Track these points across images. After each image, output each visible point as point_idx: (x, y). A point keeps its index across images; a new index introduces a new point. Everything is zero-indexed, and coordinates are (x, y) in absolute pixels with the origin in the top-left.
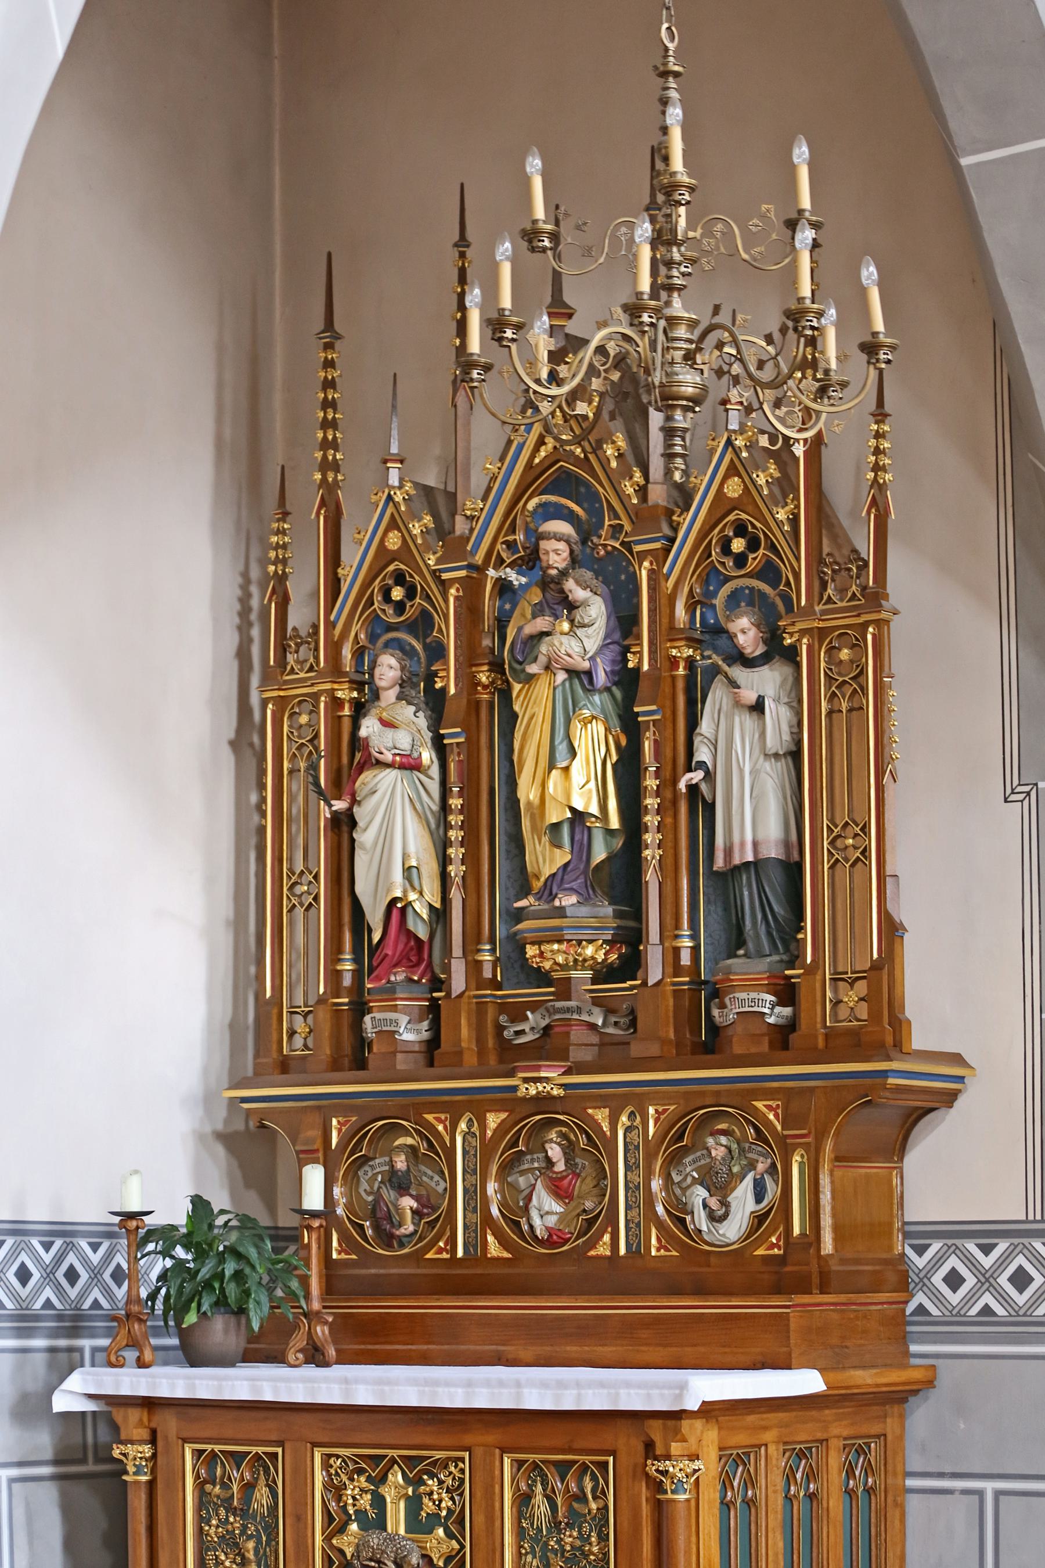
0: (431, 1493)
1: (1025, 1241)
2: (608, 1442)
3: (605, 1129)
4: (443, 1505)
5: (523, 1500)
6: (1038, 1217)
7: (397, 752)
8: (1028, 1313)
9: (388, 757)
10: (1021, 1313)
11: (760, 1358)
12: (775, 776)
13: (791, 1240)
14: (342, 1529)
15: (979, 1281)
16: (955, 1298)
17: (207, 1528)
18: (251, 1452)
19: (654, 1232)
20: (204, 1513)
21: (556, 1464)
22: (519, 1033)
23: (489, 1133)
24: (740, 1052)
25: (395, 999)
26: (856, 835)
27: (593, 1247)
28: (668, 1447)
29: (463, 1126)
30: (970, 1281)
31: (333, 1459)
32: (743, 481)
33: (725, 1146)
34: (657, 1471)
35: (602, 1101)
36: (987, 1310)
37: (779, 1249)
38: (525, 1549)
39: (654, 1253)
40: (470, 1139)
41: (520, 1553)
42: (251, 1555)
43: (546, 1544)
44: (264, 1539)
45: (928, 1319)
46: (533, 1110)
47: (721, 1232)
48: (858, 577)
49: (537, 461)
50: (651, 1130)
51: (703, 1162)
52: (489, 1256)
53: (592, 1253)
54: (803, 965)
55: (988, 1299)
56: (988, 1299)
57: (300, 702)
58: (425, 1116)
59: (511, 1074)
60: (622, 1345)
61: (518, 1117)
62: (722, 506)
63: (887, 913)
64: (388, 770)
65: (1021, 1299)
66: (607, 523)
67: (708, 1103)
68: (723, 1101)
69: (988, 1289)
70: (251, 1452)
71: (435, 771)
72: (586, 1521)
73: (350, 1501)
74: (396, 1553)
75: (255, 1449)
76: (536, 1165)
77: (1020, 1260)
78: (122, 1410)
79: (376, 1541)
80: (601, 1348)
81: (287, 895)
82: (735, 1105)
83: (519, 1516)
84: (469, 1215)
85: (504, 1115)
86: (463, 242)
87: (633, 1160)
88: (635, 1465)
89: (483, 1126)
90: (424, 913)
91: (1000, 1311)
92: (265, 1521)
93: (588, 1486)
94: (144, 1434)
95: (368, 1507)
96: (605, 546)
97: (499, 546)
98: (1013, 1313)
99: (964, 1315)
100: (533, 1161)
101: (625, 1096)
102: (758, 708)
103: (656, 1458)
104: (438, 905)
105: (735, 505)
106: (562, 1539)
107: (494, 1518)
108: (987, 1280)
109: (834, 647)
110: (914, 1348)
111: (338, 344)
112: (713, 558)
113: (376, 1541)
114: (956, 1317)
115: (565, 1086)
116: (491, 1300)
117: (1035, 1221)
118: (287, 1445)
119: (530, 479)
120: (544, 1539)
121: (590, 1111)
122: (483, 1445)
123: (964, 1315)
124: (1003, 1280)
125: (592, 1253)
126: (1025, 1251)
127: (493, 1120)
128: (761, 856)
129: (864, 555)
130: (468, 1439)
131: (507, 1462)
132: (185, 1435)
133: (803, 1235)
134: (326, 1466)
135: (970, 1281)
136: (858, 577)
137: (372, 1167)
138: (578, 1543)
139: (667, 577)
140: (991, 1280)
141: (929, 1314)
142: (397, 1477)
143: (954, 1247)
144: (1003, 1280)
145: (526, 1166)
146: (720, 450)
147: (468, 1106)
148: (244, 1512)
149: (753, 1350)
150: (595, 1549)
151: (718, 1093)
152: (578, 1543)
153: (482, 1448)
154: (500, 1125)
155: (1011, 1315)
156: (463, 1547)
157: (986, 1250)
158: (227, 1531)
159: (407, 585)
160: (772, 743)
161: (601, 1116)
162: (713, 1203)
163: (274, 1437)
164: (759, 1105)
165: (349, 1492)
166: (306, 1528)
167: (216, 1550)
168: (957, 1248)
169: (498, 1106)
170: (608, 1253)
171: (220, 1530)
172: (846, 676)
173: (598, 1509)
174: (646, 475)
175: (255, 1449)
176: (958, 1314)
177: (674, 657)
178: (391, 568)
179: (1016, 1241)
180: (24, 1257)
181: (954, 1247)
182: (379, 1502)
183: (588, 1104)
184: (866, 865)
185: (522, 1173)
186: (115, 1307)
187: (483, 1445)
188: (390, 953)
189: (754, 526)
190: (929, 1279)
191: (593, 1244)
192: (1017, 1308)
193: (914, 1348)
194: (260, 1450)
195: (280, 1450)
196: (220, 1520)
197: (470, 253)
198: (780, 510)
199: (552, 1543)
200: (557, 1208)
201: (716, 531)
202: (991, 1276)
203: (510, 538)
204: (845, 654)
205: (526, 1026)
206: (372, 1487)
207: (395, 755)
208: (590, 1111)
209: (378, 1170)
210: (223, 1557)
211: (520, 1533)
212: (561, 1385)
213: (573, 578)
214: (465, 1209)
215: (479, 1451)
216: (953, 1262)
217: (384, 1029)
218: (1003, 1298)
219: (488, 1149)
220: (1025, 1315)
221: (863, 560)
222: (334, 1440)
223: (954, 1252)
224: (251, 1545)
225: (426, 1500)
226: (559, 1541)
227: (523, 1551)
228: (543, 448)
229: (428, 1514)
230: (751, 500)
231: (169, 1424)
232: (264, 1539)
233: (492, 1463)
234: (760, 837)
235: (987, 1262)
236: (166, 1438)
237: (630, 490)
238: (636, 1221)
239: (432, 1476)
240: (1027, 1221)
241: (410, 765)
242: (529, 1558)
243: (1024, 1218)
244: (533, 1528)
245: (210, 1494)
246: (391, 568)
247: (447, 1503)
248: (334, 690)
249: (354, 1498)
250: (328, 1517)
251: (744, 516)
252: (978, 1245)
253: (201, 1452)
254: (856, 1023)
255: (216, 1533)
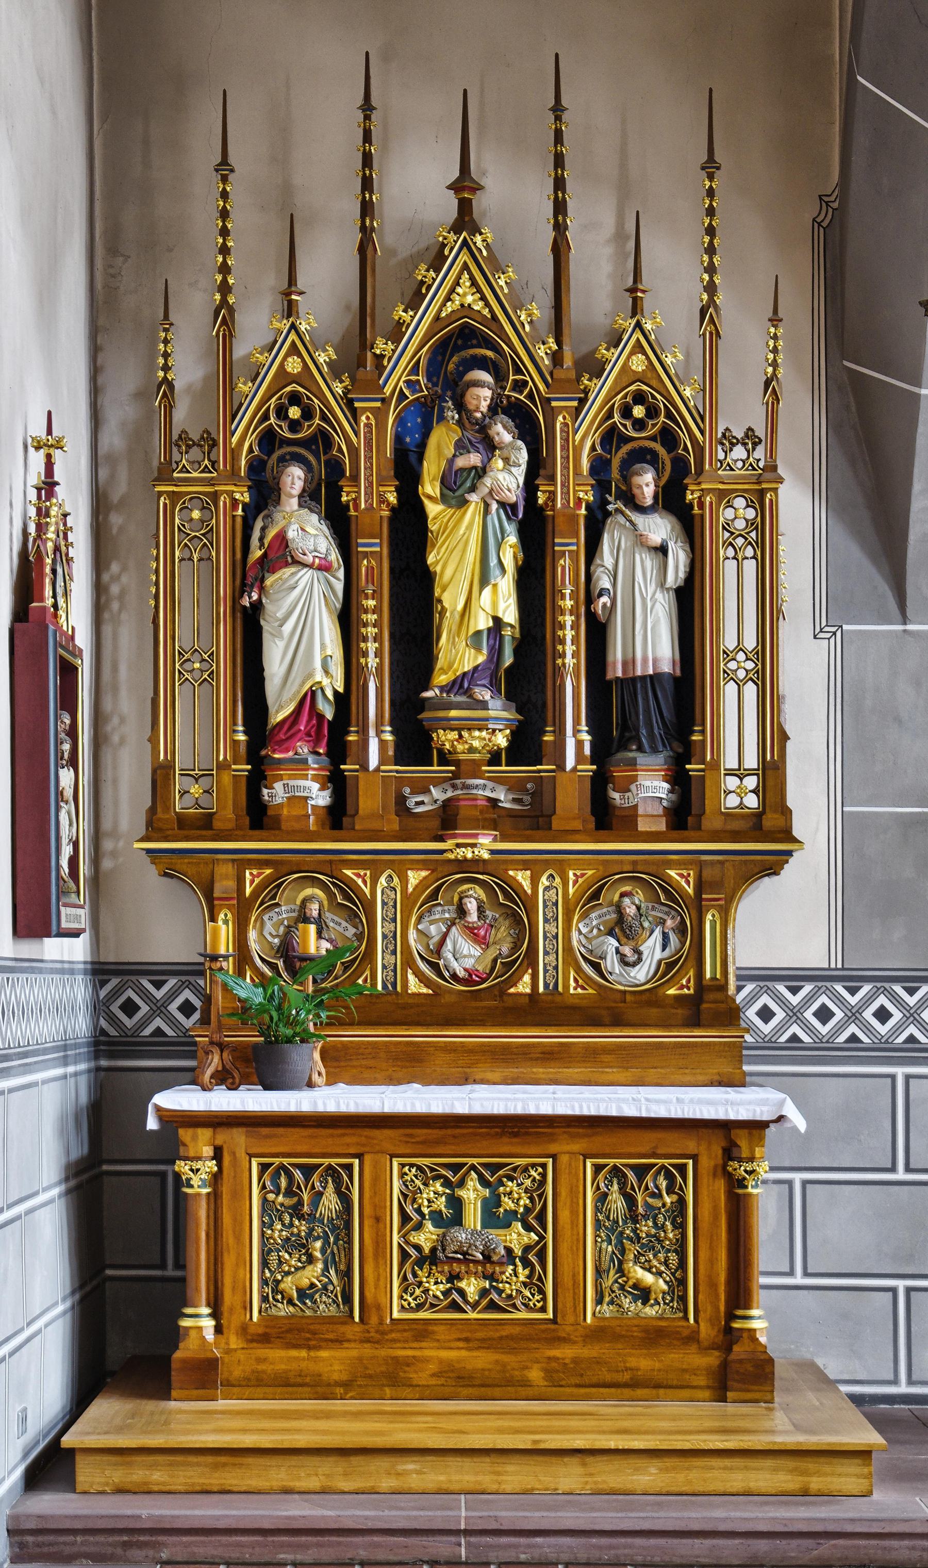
0: (511, 1193)
1: (828, 984)
2: (553, 1148)
3: (526, 888)
4: (522, 1203)
5: (602, 1198)
6: (839, 966)
7: (317, 554)
8: (890, 1041)
9: (309, 559)
10: (824, 1040)
11: (717, 1078)
12: (667, 606)
13: (704, 983)
14: (419, 1227)
15: (788, 1015)
16: (767, 1028)
17: (269, 1232)
18: (273, 1164)
19: (572, 973)
20: (266, 1219)
21: (632, 1167)
22: (418, 804)
23: (410, 889)
24: (643, 829)
25: (637, 771)
26: (203, 660)
27: (515, 985)
28: (752, 1151)
29: (383, 881)
30: (780, 1015)
31: (407, 1168)
32: (648, 358)
33: (636, 906)
34: (746, 1171)
35: (525, 866)
36: (853, 1038)
37: (689, 989)
38: (601, 1237)
39: (572, 991)
40: (389, 892)
41: (596, 1241)
42: (318, 1254)
43: (622, 1233)
44: (332, 1239)
45: (917, 1046)
46: (457, 870)
47: (632, 975)
48: (186, 453)
49: (443, 314)
50: (571, 891)
51: (608, 917)
52: (410, 992)
53: (512, 990)
54: (703, 761)
55: (795, 1029)
56: (795, 1029)
57: (191, 499)
58: (344, 871)
59: (441, 839)
60: (586, 1067)
61: (440, 875)
62: (283, 376)
63: (780, 724)
64: (306, 570)
65: (824, 1030)
66: (511, 378)
67: (625, 870)
68: (640, 868)
69: (795, 1022)
70: (273, 1164)
71: (341, 574)
72: (660, 1213)
73: (426, 1203)
74: (485, 1245)
75: (327, 1161)
76: (447, 915)
77: (130, 993)
78: (190, 1131)
79: (464, 1236)
80: (567, 1070)
81: (179, 671)
82: (651, 872)
83: (597, 1210)
84: (387, 957)
85: (424, 874)
86: (558, 109)
87: (551, 914)
88: (716, 1167)
89: (404, 881)
90: (330, 694)
91: (806, 1038)
92: (333, 1224)
93: (663, 1184)
94: (208, 1151)
95: (443, 1209)
96: (509, 397)
97: (401, 383)
98: (817, 1040)
99: (775, 1042)
100: (443, 912)
101: (547, 862)
102: (662, 550)
103: (740, 1160)
104: (341, 690)
105: (295, 379)
106: (637, 1229)
107: (578, 1213)
108: (795, 1014)
109: (187, 507)
110: (746, 1068)
111: (231, 177)
112: (272, 420)
113: (464, 1236)
114: (769, 1044)
115: (492, 852)
116: (462, 1030)
117: (836, 969)
118: (368, 1158)
119: (436, 330)
120: (620, 1229)
121: (511, 873)
122: (568, 1153)
123: (775, 1042)
124: (809, 1015)
125: (512, 990)
126: (828, 992)
127: (414, 877)
128: (659, 671)
129: (214, 435)
130: (553, 1148)
131: (589, 1165)
132: (253, 1151)
133: (714, 978)
134: (402, 1175)
135: (780, 1015)
136: (186, 453)
137: (278, 914)
138: (653, 1231)
139: (233, 434)
140: (798, 1014)
141: (860, 1041)
142: (473, 1182)
143: (882, 989)
144: (839, 1014)
145: (437, 916)
146: (630, 330)
147: (390, 864)
148: (311, 1219)
149: (711, 1071)
150: (671, 1235)
151: (635, 863)
152: (653, 1231)
153: (567, 1155)
154: (421, 881)
155: (178, 1036)
156: (542, 1238)
157: (158, 985)
158: (292, 1234)
159: (302, 406)
160: (671, 581)
161: (523, 878)
162: (627, 950)
163: (352, 1151)
164: (672, 873)
165: (425, 1195)
166: (385, 1228)
167: (278, 1251)
168: (769, 988)
169: (424, 865)
170: (528, 990)
171: (284, 1233)
172: (198, 531)
173: (672, 1203)
174: (559, 342)
175: (327, 1161)
176: (887, 1042)
177: (236, 500)
178: (288, 389)
179: (820, 984)
180: (130, 993)
181: (882, 989)
182: (456, 1203)
183: (510, 867)
184: (213, 686)
185: (432, 922)
186: (123, 1034)
187: (568, 1153)
188: (302, 728)
189: (654, 397)
190: (166, 1008)
191: (514, 980)
192: (820, 1037)
193: (746, 1068)
194: (333, 1161)
195: (356, 1162)
196: (283, 1225)
197: (565, 117)
198: (687, 388)
199: (628, 1232)
200: (476, 951)
201: (274, 399)
202: (799, 1011)
203: (413, 378)
204: (196, 514)
205: (426, 798)
206: (447, 1191)
207: (314, 557)
208: (511, 873)
209: (284, 916)
210: (287, 1256)
211: (598, 1224)
212: (710, 1103)
213: (502, 423)
214: (383, 952)
215: (564, 1159)
216: (882, 1000)
217: (297, 794)
218: (867, 1028)
219: (409, 900)
220: (827, 1042)
221: (213, 440)
222: (417, 1152)
223: (765, 992)
224: (318, 1244)
225: (505, 1199)
226: (635, 1231)
227: (599, 1240)
228: (449, 304)
229: (506, 1210)
230: (654, 375)
231: (238, 1139)
232: (332, 1239)
233: (577, 1168)
234: (659, 654)
235: (795, 1000)
236: (234, 1154)
237: (541, 353)
238: (554, 964)
239: (511, 1179)
240: (830, 969)
241: (325, 567)
242: (604, 1245)
243: (827, 966)
244: (609, 1220)
245: (273, 1202)
246: (288, 389)
247: (525, 1201)
248: (233, 492)
249: (429, 1201)
250: (405, 1218)
251: (645, 388)
252: (844, 987)
253: (268, 1166)
254: (747, 810)
255: (280, 1237)
